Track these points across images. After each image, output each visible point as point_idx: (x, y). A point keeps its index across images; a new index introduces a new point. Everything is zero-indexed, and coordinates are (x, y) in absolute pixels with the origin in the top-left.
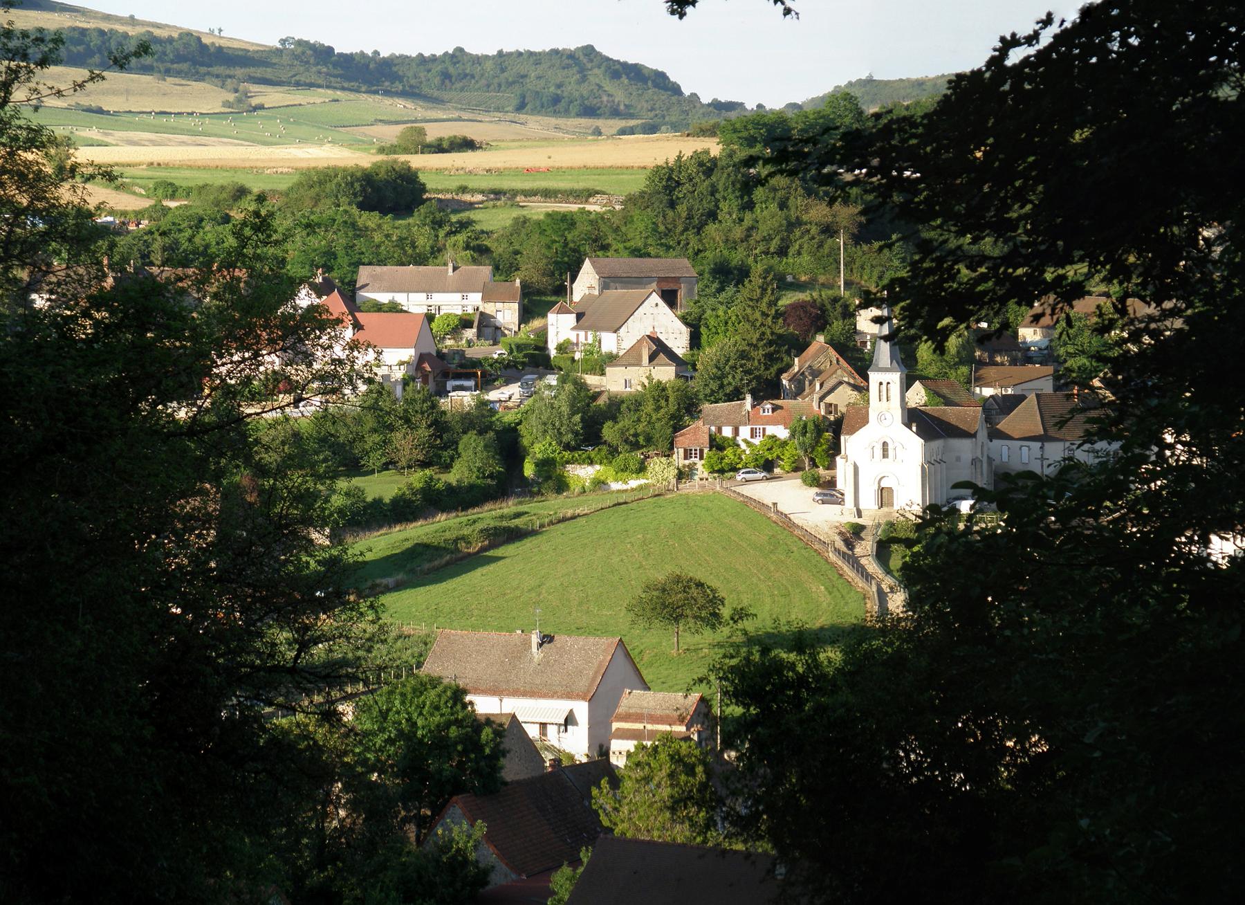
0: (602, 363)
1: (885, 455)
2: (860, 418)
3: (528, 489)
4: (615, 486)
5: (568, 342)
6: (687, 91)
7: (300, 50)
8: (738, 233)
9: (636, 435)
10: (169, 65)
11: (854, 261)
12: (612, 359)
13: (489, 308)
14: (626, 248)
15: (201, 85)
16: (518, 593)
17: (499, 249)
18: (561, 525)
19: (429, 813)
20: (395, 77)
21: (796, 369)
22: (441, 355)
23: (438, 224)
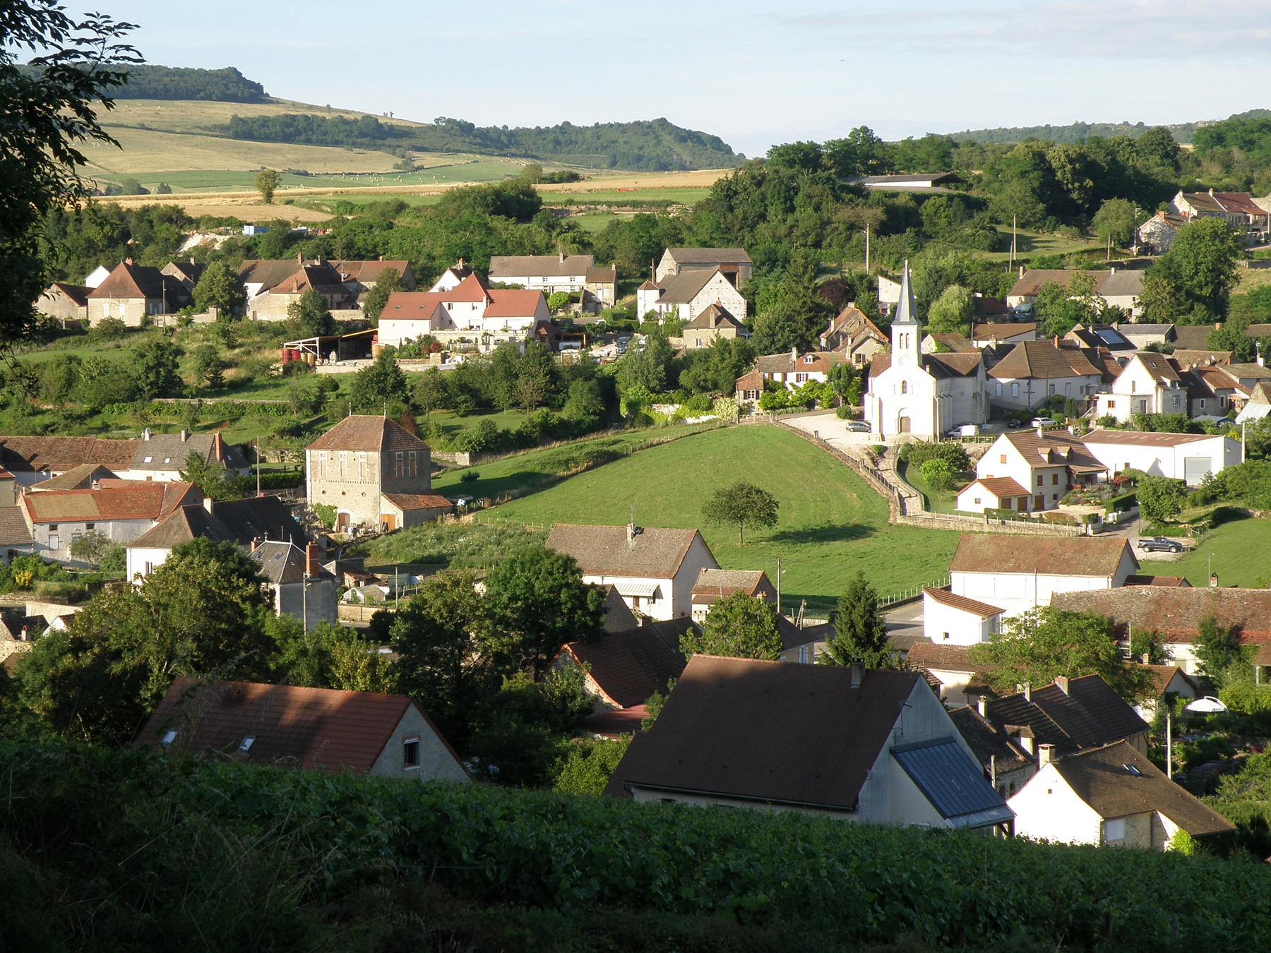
0: (679, 327)
1: (904, 392)
2: (884, 363)
3: (620, 423)
4: (690, 421)
5: (653, 312)
6: (736, 152)
7: (449, 126)
8: (783, 230)
9: (705, 381)
10: (355, 139)
11: (876, 250)
12: (686, 324)
13: (592, 288)
14: (697, 241)
15: (379, 153)
16: (616, 501)
17: (599, 245)
18: (649, 450)
19: (545, 657)
20: (518, 144)
21: (832, 329)
22: (554, 322)
23: (550, 227)
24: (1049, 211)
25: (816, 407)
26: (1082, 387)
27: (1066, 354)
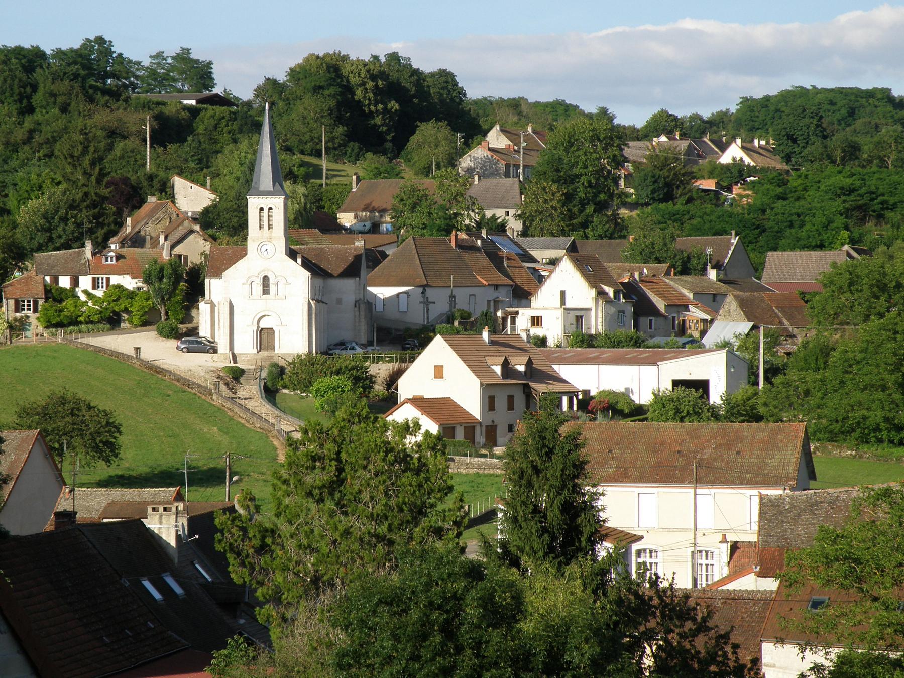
1: (266, 291)
21: (129, 230)
24: (350, 136)
25: (122, 325)
26: (489, 302)
27: (467, 256)
